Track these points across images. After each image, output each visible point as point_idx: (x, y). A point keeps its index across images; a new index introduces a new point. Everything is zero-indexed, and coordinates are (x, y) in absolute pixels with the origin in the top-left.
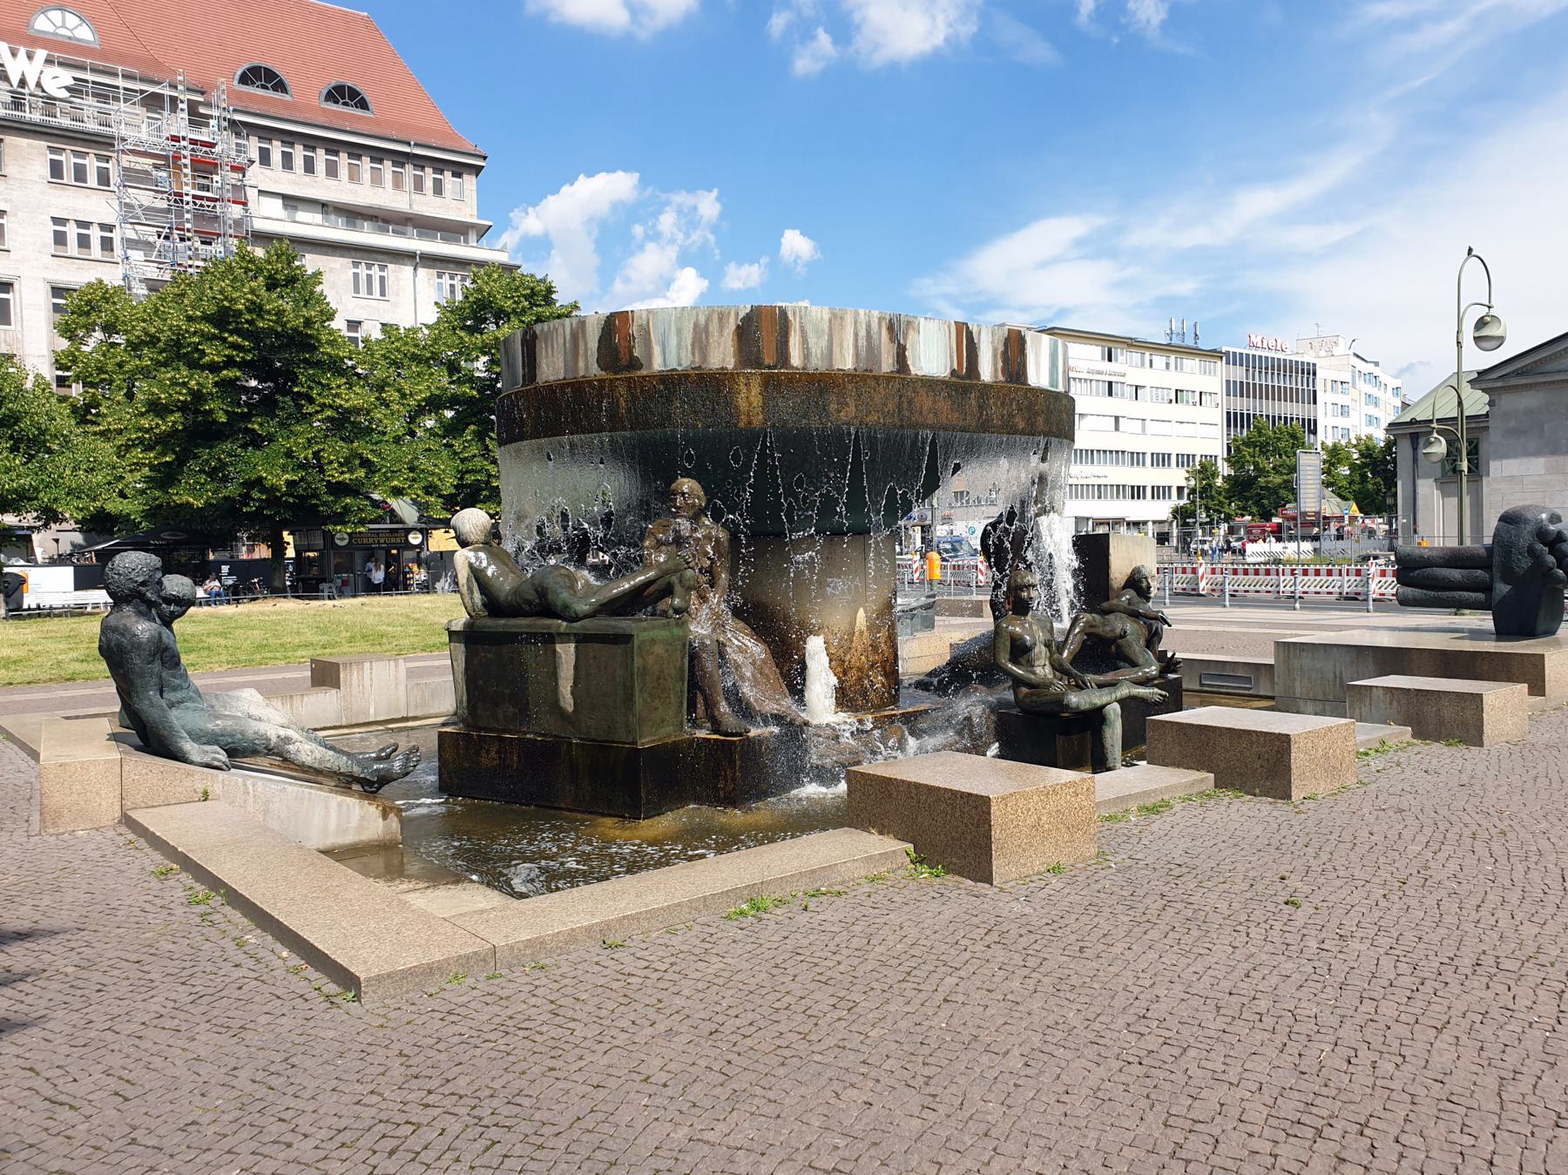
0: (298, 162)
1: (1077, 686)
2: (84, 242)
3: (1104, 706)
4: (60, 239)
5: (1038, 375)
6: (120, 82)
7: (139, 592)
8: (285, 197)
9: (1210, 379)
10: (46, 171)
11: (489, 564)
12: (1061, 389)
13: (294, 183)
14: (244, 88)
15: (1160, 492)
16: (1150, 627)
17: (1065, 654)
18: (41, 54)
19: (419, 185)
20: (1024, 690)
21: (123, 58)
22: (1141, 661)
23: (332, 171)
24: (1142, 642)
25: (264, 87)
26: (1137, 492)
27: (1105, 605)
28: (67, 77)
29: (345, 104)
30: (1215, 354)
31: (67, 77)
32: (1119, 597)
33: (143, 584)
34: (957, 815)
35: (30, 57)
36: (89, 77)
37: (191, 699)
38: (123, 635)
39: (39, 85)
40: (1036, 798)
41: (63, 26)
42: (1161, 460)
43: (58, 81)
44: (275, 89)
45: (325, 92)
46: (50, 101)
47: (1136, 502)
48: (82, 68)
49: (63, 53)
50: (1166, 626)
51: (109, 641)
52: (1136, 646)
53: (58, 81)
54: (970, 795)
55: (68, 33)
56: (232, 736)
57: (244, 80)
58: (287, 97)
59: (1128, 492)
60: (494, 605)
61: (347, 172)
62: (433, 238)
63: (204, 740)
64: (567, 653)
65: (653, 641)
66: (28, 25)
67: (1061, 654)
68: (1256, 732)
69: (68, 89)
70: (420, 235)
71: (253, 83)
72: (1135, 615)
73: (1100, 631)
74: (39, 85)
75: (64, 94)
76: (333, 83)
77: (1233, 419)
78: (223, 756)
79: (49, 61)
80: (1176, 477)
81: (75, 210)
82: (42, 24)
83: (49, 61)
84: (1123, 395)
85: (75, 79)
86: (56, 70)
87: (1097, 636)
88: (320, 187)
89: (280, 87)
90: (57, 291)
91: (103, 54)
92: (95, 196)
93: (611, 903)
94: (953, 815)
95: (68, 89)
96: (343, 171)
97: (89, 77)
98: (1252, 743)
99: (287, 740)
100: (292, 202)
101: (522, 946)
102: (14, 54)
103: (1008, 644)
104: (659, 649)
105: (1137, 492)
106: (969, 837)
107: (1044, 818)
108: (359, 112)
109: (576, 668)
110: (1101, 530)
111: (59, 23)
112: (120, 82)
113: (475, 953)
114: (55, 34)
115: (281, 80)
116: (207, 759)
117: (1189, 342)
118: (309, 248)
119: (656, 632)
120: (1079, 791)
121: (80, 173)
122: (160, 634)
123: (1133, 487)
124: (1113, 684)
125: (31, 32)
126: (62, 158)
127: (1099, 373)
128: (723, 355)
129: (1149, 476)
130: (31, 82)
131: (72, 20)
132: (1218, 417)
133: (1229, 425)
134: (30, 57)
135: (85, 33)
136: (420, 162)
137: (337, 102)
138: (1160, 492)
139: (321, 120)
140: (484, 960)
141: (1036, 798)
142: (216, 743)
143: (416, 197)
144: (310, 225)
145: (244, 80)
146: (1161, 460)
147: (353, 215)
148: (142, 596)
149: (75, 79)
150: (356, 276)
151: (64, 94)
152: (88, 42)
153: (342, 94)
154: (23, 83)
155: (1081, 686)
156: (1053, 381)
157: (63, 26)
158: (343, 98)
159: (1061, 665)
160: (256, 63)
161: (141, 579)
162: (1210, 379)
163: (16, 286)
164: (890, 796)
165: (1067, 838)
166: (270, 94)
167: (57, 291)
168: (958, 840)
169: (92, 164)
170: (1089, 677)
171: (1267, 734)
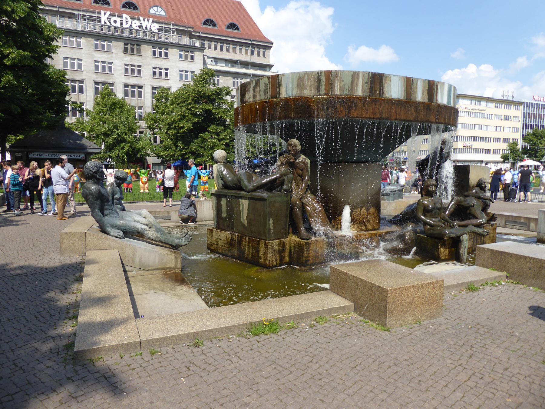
0: (218, 47)
1: (450, 226)
2: (161, 74)
3: (460, 236)
4: (155, 73)
5: (442, 99)
6: (171, 27)
7: (93, 175)
8: (215, 58)
9: (518, 113)
10: (151, 54)
11: (224, 170)
12: (452, 105)
13: (217, 54)
14: (205, 26)
15: (496, 151)
16: (485, 203)
17: (447, 212)
18: (151, 20)
19: (253, 53)
20: (428, 227)
21: (172, 19)
22: (479, 217)
23: (234, 51)
24: (480, 209)
25: (210, 25)
26: (488, 151)
27: (466, 193)
28: (157, 26)
29: (233, 29)
30: (520, 103)
31: (157, 26)
32: (472, 190)
33: (95, 172)
34: (373, 294)
35: (148, 21)
36: (163, 26)
37: (112, 213)
38: (87, 190)
39: (150, 28)
40: (412, 290)
41: (157, 11)
42: (497, 140)
43: (155, 27)
44: (213, 26)
45: (227, 26)
46: (154, 34)
47: (487, 155)
48: (161, 23)
49: (157, 19)
50: (491, 203)
51: (84, 191)
52: (477, 210)
53: (155, 27)
54: (379, 286)
55: (159, 13)
56: (125, 227)
57: (205, 24)
58: (216, 28)
59: (484, 151)
60: (226, 186)
61: (232, 50)
62: (256, 70)
63: (116, 228)
64: (245, 203)
65: (275, 202)
66: (149, 12)
67: (445, 213)
68: (529, 257)
69: (158, 29)
70: (260, 70)
71: (207, 25)
72: (479, 198)
73: (463, 204)
74: (150, 28)
75: (157, 31)
76: (229, 23)
77: (525, 126)
78: (121, 234)
79: (153, 22)
80: (503, 146)
81: (159, 65)
82: (152, 11)
83: (153, 22)
84: (484, 117)
85: (160, 26)
86: (155, 24)
87: (461, 205)
88: (225, 55)
89: (214, 25)
90: (154, 88)
91: (167, 19)
92: (164, 60)
93: (205, 321)
94: (371, 294)
95: (158, 29)
96: (231, 50)
97: (163, 26)
98: (527, 262)
99: (145, 230)
100: (216, 60)
101: (154, 341)
102: (144, 20)
103: (422, 208)
104: (277, 205)
105: (488, 151)
106: (377, 305)
107: (416, 299)
108: (236, 31)
109: (248, 210)
110: (467, 164)
111: (156, 11)
112: (171, 27)
113: (131, 343)
114: (155, 14)
115: (211, 20)
116: (116, 235)
117: (510, 98)
118: (221, 73)
119: (276, 198)
120: (435, 286)
121: (160, 54)
122: (100, 191)
123: (486, 149)
124: (465, 226)
125: (149, 14)
126: (156, 50)
127: (476, 110)
128: (309, 92)
129: (492, 146)
130: (148, 28)
131: (160, 9)
132: (519, 125)
133: (523, 129)
134: (148, 21)
135: (163, 13)
136: (254, 46)
137: (230, 29)
138: (496, 151)
139: (225, 34)
140: (136, 346)
141: (412, 290)
142: (118, 229)
143: (252, 57)
144: (221, 67)
145: (205, 24)
146: (497, 140)
147: (234, 63)
148: (95, 177)
149: (160, 26)
150: (234, 82)
151: (157, 31)
152: (163, 15)
153: (232, 26)
154: (146, 28)
155: (452, 227)
156: (449, 101)
157: (157, 11)
158: (232, 27)
159: (444, 217)
160: (208, 18)
161: (94, 171)
162: (518, 113)
163: (143, 87)
164: (346, 281)
165: (427, 308)
166: (211, 27)
167: (154, 88)
168: (373, 306)
169: (163, 51)
170: (455, 223)
171: (534, 259)
